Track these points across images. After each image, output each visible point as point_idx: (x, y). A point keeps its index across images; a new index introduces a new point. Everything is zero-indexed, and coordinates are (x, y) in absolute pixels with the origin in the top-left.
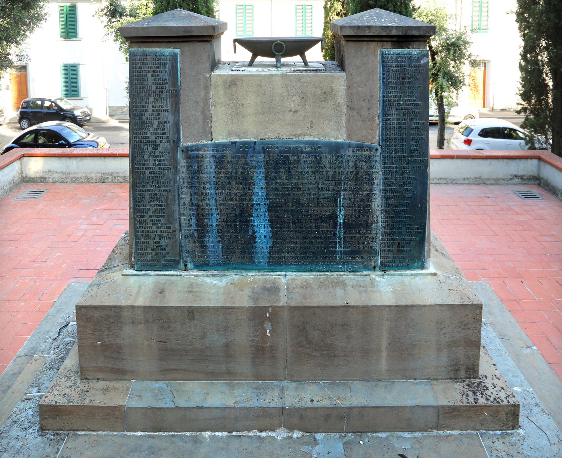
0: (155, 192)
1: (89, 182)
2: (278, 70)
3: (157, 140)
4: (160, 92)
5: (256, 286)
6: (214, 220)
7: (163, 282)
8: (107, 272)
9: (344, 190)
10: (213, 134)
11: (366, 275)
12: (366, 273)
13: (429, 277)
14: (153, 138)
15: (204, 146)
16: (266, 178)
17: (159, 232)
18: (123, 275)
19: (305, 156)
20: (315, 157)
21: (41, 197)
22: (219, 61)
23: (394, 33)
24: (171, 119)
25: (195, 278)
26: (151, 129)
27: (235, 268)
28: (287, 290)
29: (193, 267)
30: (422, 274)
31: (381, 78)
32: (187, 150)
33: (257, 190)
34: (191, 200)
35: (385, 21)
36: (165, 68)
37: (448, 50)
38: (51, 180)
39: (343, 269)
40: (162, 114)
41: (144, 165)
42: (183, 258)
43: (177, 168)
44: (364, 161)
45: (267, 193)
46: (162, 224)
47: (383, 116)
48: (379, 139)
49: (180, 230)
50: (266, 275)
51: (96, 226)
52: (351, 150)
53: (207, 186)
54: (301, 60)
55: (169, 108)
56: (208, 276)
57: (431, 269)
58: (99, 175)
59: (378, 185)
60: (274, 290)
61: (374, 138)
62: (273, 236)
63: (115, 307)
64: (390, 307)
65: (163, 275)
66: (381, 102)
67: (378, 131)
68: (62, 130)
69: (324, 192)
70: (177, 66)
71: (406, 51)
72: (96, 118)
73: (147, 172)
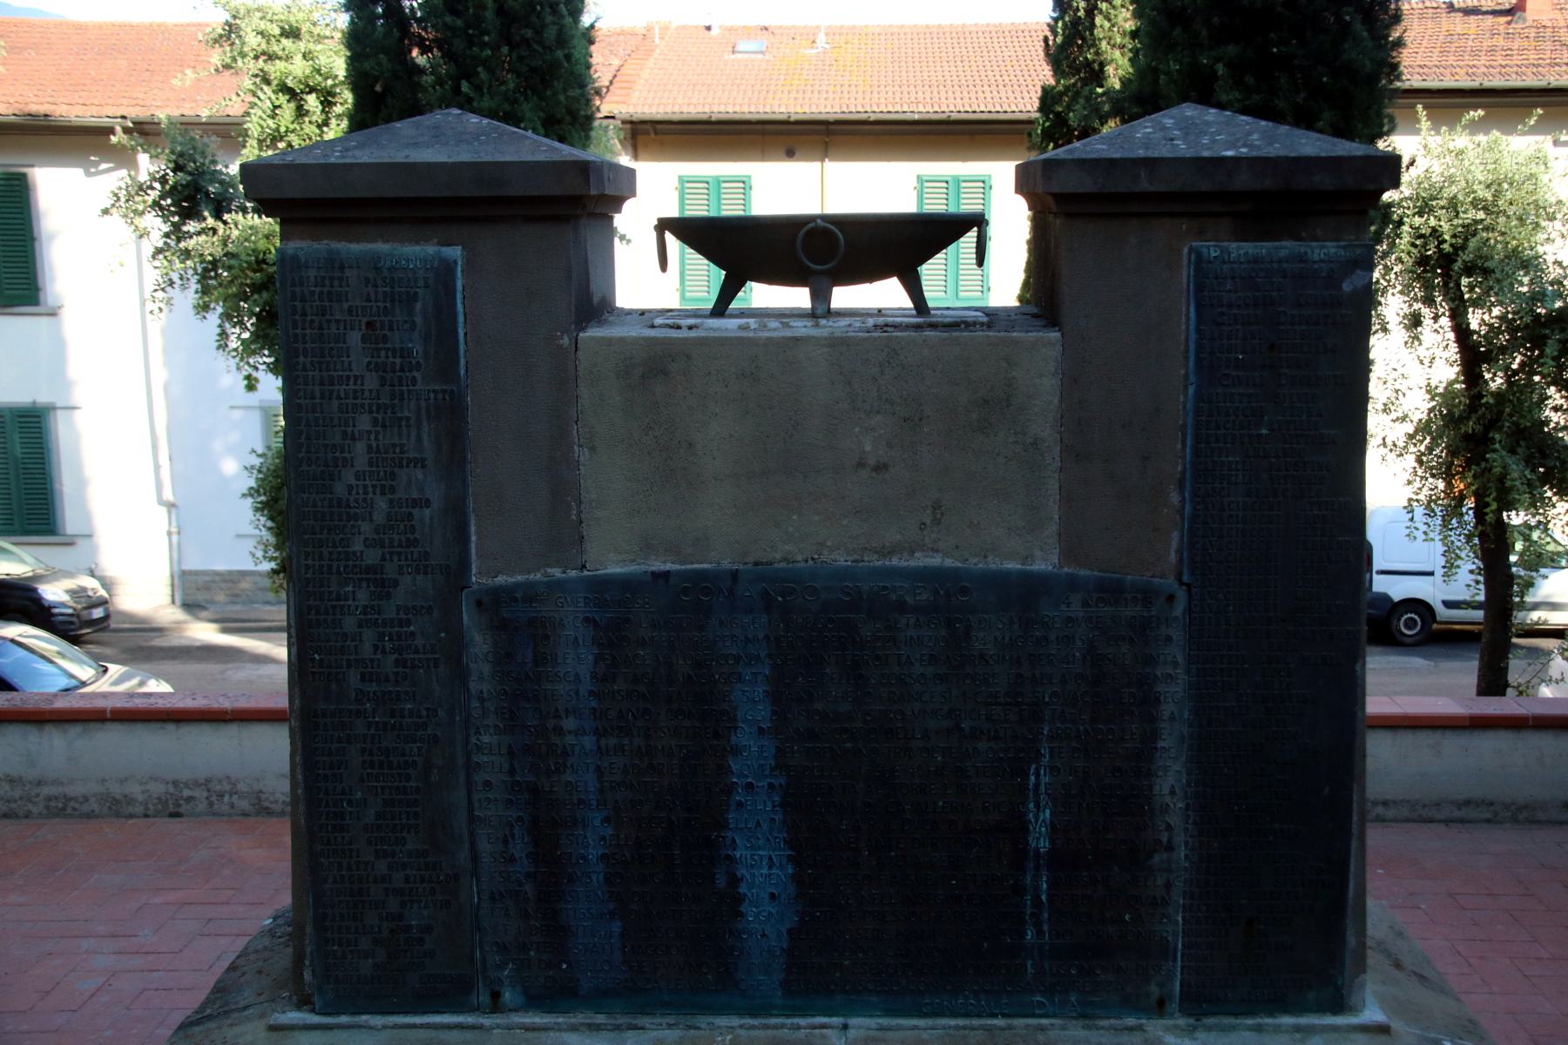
1: (117, 815)
2: (817, 325)
6: (592, 841)
8: (212, 1025)
11: (1131, 1029)
12: (1131, 1021)
14: (372, 557)
15: (554, 585)
18: (273, 1028)
19: (912, 622)
23: (1243, 181)
24: (435, 491)
25: (530, 1035)
26: (365, 527)
29: (520, 1000)
31: (1192, 346)
32: (494, 603)
33: (744, 737)
34: (512, 772)
35: (1214, 141)
37: (1538, 342)
45: (778, 749)
48: (1181, 561)
50: (776, 1027)
51: (150, 958)
53: (569, 723)
54: (907, 303)
56: (573, 1028)
58: (157, 789)
59: (1172, 719)
61: (1163, 557)
65: (414, 1026)
66: (1190, 431)
67: (1175, 535)
69: (982, 745)
70: (455, 305)
71: (1286, 247)
73: (353, 677)
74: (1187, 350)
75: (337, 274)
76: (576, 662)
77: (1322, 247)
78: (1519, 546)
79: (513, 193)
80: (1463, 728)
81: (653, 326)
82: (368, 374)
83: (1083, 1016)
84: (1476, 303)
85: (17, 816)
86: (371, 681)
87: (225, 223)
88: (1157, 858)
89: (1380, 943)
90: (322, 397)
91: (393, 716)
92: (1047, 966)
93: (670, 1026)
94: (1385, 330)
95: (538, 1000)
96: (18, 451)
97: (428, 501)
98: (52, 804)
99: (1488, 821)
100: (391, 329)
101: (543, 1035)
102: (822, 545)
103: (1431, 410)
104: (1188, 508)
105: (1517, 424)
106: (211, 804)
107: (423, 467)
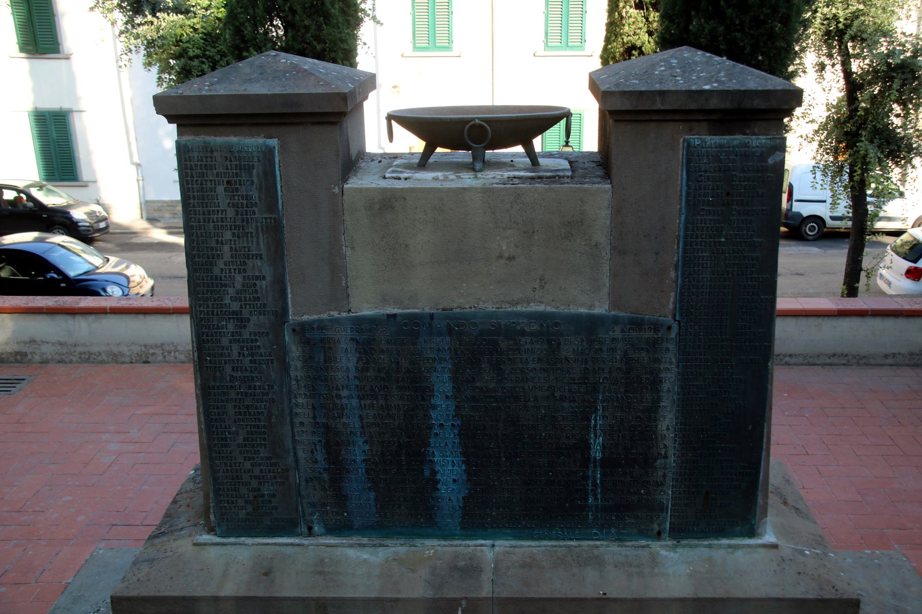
0: (246, 403)
1: (117, 362)
2: (476, 177)
3: (244, 310)
4: (243, 221)
5: (439, 563)
6: (358, 452)
7: (270, 556)
8: (165, 538)
9: (603, 401)
10: (351, 299)
11: (643, 547)
13: (762, 550)
14: (235, 306)
16: (454, 380)
17: (257, 471)
18: (195, 544)
19: (528, 340)
20: (549, 342)
21: (20, 390)
22: (362, 154)
23: (714, 103)
25: (328, 549)
26: (231, 290)
27: (400, 534)
28: (496, 571)
29: (323, 531)
30: (749, 546)
31: (684, 193)
32: (302, 330)
33: (438, 400)
34: (315, 417)
35: (699, 77)
36: (251, 175)
38: (37, 358)
39: (601, 536)
40: (250, 263)
41: (222, 355)
42: (304, 516)
43: (284, 361)
44: (643, 349)
46: (262, 458)
47: (684, 265)
48: (675, 309)
49: (297, 468)
50: (457, 546)
51: (138, 445)
52: (618, 329)
53: (344, 393)
55: (264, 252)
56: (351, 546)
57: (770, 538)
58: (136, 349)
59: (669, 391)
60: (472, 570)
61: (665, 306)
62: (468, 480)
63: (184, 598)
64: (682, 601)
65: (268, 544)
66: (682, 239)
67: (673, 294)
68: (50, 250)
69: (565, 405)
72: (119, 226)
73: (228, 369)
74: (681, 195)
75: (209, 155)
76: (347, 361)
77: (758, 139)
78: (873, 186)
79: (303, 110)
80: (834, 316)
81: (385, 178)
82: (228, 209)
83: (619, 540)
84: (857, 56)
85: (66, 362)
86: (237, 371)
87: (158, 18)
88: (658, 462)
89: (777, 488)
90: (204, 221)
91: (250, 388)
92: (599, 515)
93: (401, 545)
94: (804, 72)
95: (331, 530)
96: (55, 135)
97: (264, 277)
98: (83, 356)
99: (844, 364)
100: (240, 184)
101: (335, 549)
102: (479, 299)
103: (828, 117)
104: (679, 280)
105: (875, 126)
106: (165, 357)
107: (261, 259)
